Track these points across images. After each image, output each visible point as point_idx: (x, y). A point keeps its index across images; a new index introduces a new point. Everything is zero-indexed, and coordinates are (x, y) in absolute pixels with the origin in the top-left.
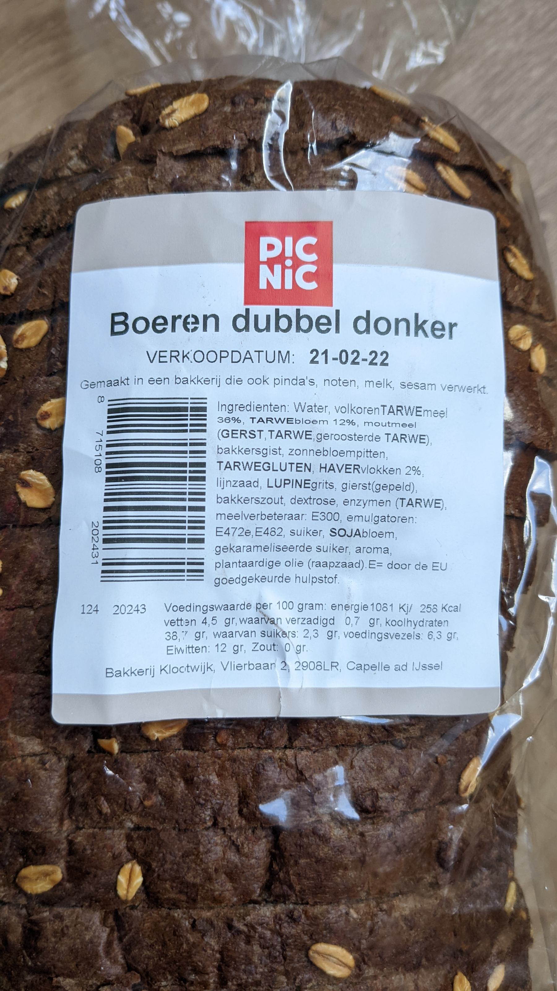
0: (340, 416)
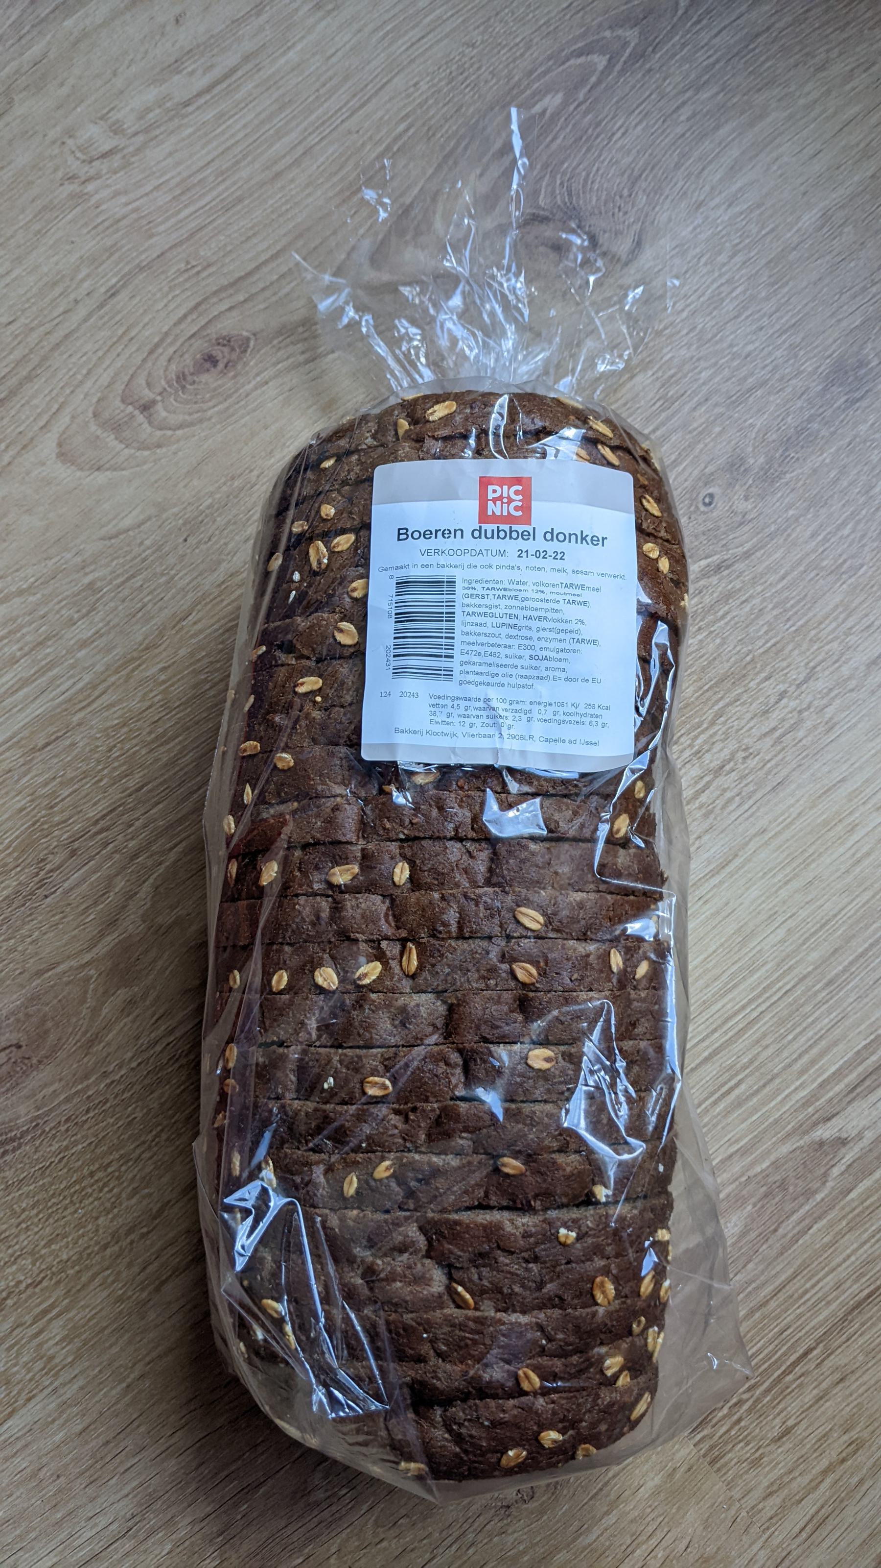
0: (535, 588)
